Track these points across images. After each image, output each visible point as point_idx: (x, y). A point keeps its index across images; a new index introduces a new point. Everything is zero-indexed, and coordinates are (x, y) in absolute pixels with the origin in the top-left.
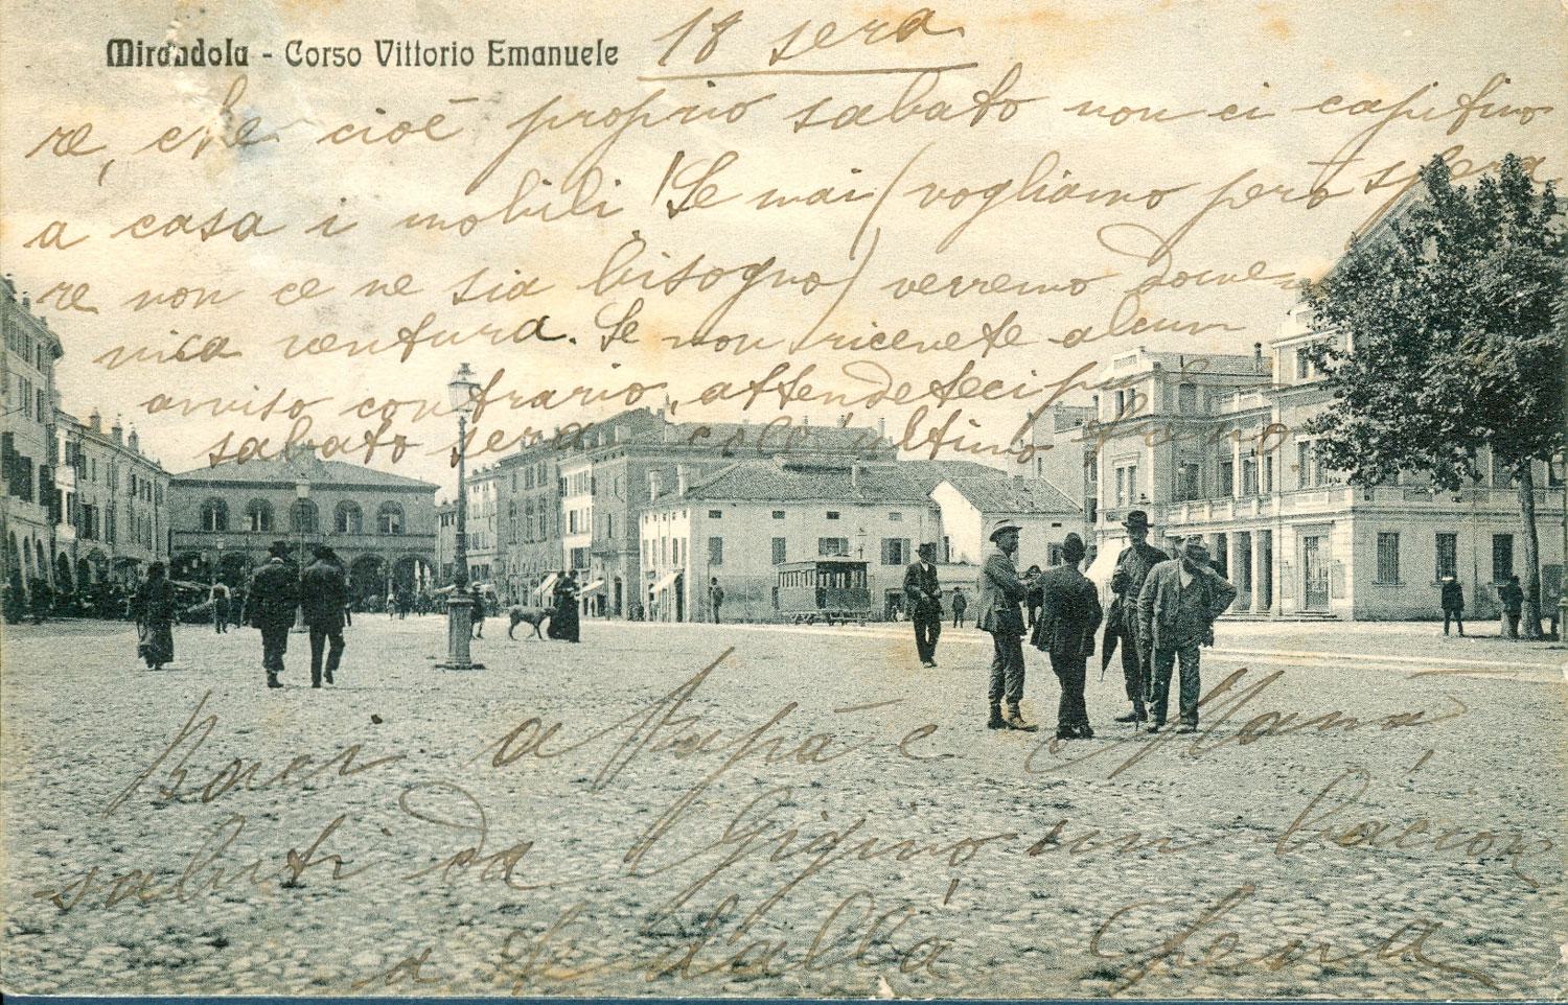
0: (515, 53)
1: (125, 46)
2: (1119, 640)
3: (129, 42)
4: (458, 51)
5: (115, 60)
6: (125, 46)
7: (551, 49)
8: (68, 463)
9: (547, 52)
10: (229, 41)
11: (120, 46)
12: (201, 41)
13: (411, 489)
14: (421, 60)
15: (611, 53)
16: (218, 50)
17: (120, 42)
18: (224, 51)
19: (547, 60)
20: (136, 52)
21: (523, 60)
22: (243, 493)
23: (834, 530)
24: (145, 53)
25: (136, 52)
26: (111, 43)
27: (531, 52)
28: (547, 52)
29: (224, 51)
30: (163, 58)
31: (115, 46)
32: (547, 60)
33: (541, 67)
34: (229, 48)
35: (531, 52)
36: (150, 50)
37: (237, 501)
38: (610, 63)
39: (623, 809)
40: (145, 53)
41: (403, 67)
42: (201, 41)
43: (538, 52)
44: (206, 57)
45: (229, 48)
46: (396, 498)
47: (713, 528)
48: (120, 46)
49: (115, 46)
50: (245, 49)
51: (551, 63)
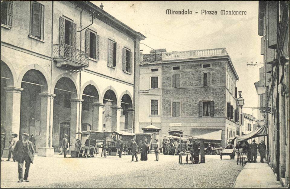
0: (168, 11)
1: (170, 11)
4: (184, 12)
5: (168, 13)
6: (170, 11)
8: (13, 158)
12: (183, 10)
14: (233, 14)
16: (187, 11)
17: (169, 10)
18: (188, 12)
19: (236, 14)
20: (171, 12)
23: (255, 121)
24: (173, 12)
25: (171, 12)
26: (167, 10)
29: (188, 12)
31: (222, 11)
32: (236, 14)
33: (179, 11)
34: (188, 11)
36: (174, 11)
39: (147, 59)
40: (173, 12)
41: (231, 15)
42: (183, 10)
43: (234, 12)
44: (184, 13)
45: (188, 11)
49: (222, 11)
51: (237, 14)
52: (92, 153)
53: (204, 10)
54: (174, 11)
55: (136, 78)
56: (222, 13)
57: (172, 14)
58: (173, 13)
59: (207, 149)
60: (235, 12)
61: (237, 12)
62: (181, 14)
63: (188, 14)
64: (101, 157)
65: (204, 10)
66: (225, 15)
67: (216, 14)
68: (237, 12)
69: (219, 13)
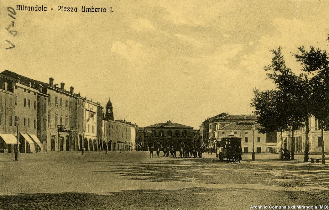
0: (18, 6)
1: (20, 6)
2: (170, 152)
3: (21, 5)
7: (32, 7)
9: (31, 8)
10: (43, 6)
11: (19, 7)
12: (37, 6)
13: (187, 128)
15: (96, 9)
16: (40, 7)
18: (42, 8)
21: (32, 10)
22: (158, 129)
27: (95, 9)
28: (31, 8)
29: (42, 8)
30: (76, 10)
32: (31, 9)
35: (95, 9)
36: (26, 7)
37: (173, 131)
38: (96, 12)
40: (24, 8)
42: (37, 6)
44: (38, 9)
46: (179, 130)
47: (278, 151)
48: (19, 7)
50: (46, 8)
51: (32, 10)
52: (183, 208)
53: (60, 6)
54: (26, 7)
55: (30, 139)
56: (88, 11)
57: (21, 10)
58: (24, 9)
59: (170, 152)
60: (30, 7)
61: (32, 8)
62: (34, 10)
63: (42, 10)
64: (212, 154)
65: (60, 6)
66: (42, 11)
67: (46, 10)
68: (32, 8)
69: (80, 9)
